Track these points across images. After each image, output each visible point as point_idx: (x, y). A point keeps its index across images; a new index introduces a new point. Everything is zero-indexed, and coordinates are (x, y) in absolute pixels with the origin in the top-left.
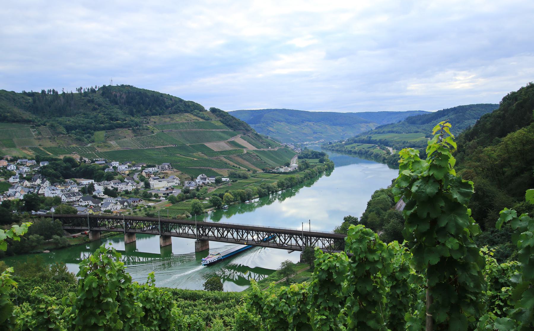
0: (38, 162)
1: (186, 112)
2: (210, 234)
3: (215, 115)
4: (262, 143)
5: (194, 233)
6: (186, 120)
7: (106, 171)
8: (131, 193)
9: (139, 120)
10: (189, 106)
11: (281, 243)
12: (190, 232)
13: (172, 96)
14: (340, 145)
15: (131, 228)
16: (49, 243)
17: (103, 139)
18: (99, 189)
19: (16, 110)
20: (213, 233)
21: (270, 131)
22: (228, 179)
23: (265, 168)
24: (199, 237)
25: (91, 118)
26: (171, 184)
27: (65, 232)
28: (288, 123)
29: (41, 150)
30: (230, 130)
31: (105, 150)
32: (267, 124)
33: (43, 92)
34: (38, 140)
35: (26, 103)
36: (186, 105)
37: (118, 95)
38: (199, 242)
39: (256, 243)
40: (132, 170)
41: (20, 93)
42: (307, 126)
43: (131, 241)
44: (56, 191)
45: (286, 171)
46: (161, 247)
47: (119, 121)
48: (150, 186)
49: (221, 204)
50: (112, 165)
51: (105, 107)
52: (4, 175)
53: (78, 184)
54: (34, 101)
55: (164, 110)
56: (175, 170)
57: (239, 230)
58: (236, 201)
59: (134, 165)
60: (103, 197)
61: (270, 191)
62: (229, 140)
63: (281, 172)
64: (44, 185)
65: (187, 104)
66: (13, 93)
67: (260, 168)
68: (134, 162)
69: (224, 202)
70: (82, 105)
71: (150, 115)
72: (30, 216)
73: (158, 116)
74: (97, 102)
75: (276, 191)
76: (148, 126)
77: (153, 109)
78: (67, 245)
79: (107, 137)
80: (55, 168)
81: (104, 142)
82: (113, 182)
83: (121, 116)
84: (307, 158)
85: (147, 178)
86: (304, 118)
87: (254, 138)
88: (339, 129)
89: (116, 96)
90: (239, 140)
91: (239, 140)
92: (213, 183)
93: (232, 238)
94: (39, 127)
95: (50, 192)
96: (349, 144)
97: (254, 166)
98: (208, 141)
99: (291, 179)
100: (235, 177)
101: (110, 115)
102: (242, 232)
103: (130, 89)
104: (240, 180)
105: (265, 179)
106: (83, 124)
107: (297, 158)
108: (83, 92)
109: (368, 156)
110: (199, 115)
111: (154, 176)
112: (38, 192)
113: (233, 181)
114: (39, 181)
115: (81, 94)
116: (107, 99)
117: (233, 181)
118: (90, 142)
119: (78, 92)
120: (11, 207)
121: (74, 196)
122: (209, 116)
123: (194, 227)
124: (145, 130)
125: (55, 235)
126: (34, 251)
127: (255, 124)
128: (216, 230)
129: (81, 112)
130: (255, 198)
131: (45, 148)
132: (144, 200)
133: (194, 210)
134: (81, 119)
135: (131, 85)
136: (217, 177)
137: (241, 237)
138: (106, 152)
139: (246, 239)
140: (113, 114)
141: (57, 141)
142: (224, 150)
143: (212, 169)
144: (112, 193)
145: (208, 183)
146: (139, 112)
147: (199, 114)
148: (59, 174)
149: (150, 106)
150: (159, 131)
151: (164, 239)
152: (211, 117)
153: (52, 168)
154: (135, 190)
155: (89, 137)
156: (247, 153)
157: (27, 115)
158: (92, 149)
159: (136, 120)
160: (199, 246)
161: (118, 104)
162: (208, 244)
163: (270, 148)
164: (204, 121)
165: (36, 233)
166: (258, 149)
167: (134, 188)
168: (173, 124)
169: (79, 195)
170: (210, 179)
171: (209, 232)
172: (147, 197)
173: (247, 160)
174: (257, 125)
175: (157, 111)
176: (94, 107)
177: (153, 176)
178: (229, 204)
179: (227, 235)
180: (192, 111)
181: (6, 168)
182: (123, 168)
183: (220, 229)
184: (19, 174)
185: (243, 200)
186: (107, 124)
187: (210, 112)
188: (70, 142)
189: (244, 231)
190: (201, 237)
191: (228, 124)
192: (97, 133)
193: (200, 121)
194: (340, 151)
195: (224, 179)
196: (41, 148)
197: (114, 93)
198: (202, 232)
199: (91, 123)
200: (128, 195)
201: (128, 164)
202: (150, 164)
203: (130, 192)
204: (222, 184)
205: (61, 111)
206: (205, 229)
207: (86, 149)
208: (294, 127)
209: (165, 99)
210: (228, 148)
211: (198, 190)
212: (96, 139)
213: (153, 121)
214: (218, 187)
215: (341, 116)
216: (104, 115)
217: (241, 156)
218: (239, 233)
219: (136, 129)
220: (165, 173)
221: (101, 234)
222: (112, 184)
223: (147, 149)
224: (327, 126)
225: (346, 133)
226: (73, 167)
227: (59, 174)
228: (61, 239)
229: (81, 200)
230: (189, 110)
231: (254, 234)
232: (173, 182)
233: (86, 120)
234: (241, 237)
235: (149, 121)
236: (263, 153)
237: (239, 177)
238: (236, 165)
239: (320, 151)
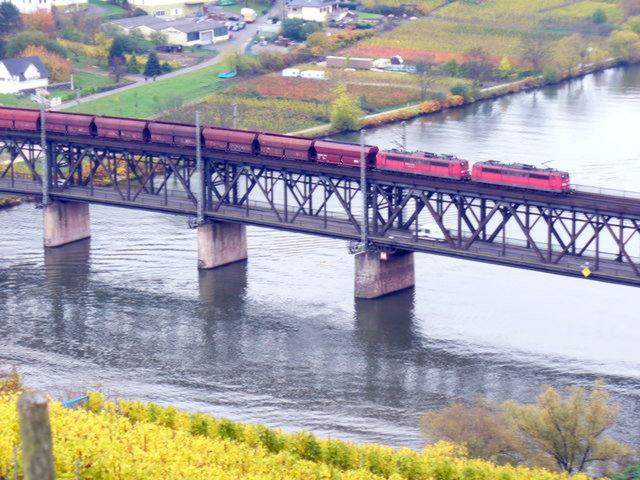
2: (257, 196)
11: (557, 248)
12: (335, 207)
15: (225, 200)
39: (280, 220)
57: (469, 200)
93: (347, 218)
102: (483, 207)
123: (272, 178)
137: (476, 226)
139: (321, 214)
162: (411, 268)
189: (490, 204)
198: (384, 213)
206: (401, 201)
218: (468, 213)
231: (533, 218)
234: (476, 226)
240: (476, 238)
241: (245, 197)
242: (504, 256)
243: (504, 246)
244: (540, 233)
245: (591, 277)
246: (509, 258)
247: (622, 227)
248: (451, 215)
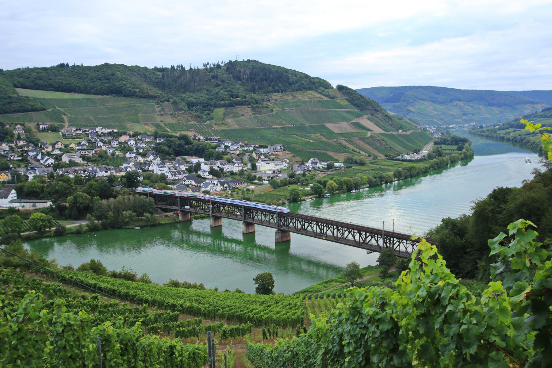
0: (156, 138)
1: (310, 89)
3: (341, 94)
4: (391, 125)
5: (333, 235)
6: (309, 98)
7: (216, 150)
8: (236, 174)
9: (260, 97)
10: (314, 83)
12: (374, 242)
13: (298, 72)
14: (492, 130)
16: (142, 220)
17: (222, 117)
18: (206, 167)
19: (145, 86)
20: (332, 232)
21: (411, 111)
22: (342, 165)
23: (388, 154)
24: (280, 227)
25: (213, 95)
26: (278, 167)
27: (159, 211)
28: (434, 102)
29: (162, 126)
30: (356, 110)
31: (222, 129)
32: (408, 103)
33: (173, 67)
34: (160, 116)
35: (156, 78)
36: (310, 82)
37: (242, 71)
38: (278, 233)
40: (243, 150)
41: (152, 69)
42: (456, 106)
43: (217, 225)
44: (164, 169)
45: (411, 159)
46: (244, 234)
47: (239, 99)
48: (256, 168)
49: (322, 192)
50: (224, 144)
51: (227, 83)
52: (123, 150)
53: (188, 162)
54: (163, 77)
55: (287, 87)
56: (287, 152)
58: (342, 189)
59: (246, 145)
60: (207, 177)
61: (383, 181)
62: (353, 121)
63: (406, 159)
64: (156, 162)
65: (312, 80)
66: (145, 69)
67: (383, 154)
68: (246, 142)
69: (327, 190)
70: (207, 81)
71: (272, 92)
72: (128, 193)
73: (280, 94)
74: (220, 78)
75: (391, 182)
76: (269, 104)
77: (276, 86)
78: (157, 223)
79: (225, 115)
80: (169, 145)
81: (223, 120)
82: (220, 162)
83: (241, 93)
84: (445, 144)
85: (256, 160)
86: (453, 97)
87: (383, 120)
88: (496, 110)
89: (240, 72)
90: (364, 121)
91: (364, 121)
92: (324, 168)
94: (163, 103)
95: (158, 169)
96: (504, 129)
97: (376, 151)
98: (330, 122)
99: (410, 169)
100: (351, 163)
101: (231, 91)
102: (366, 235)
103: (255, 64)
104: (355, 166)
105: (384, 167)
106: (204, 100)
107: (433, 143)
108: (208, 67)
109: (523, 144)
110: (323, 93)
111: (264, 157)
112: (148, 168)
113: (347, 167)
114: (151, 158)
115: (206, 69)
116: (231, 75)
117: (347, 167)
118: (208, 119)
119: (204, 68)
120: (115, 182)
121: (180, 174)
122: (334, 94)
124: (265, 109)
125: (146, 212)
126: (127, 227)
127: (394, 102)
128: (358, 234)
129: (204, 88)
130: (364, 188)
131: (166, 125)
132: (247, 182)
133: (292, 196)
134: (203, 95)
135: (257, 60)
136: (329, 162)
138: (222, 130)
140: (234, 90)
141: (178, 118)
142: (346, 132)
143: (328, 153)
144: (216, 173)
145: (319, 168)
146: (260, 88)
147: (324, 91)
148: (171, 150)
149: (273, 83)
150: (279, 109)
151: (246, 226)
152: (337, 96)
153: (167, 145)
154: (240, 172)
155: (209, 114)
156: (371, 136)
157: (154, 91)
158: (210, 126)
159: (256, 96)
160: (279, 236)
161: (241, 81)
162: (289, 235)
163: (400, 131)
164: (329, 99)
165: (130, 209)
166: (387, 131)
167: (240, 169)
168: (294, 102)
169: (184, 173)
170: (323, 163)
171: (327, 231)
172: (251, 179)
173: (369, 145)
174: (396, 104)
175: (279, 87)
176: (217, 83)
177: (263, 157)
178: (332, 193)
179: (348, 236)
180: (316, 88)
181: (127, 143)
182: (234, 148)
183: (362, 232)
184: (136, 149)
185: (349, 190)
186: (227, 101)
187: (337, 90)
188: (189, 118)
190: (282, 227)
191: (355, 103)
192: (216, 110)
193: (324, 99)
194: (490, 137)
195: (336, 164)
196: (162, 125)
197: (239, 68)
199: (212, 100)
200: (233, 176)
201: (241, 143)
202: (263, 144)
203: (236, 173)
204: (333, 169)
205: (185, 88)
207: (203, 127)
208: (440, 107)
209: (290, 75)
210: (351, 130)
211: (304, 175)
212: (215, 116)
213: (274, 99)
214: (328, 173)
215: (500, 95)
216: (226, 91)
217: (363, 139)
219: (255, 105)
220: (276, 155)
221: (191, 215)
222: (219, 164)
223: (263, 128)
224: (481, 107)
225: (504, 116)
226: (186, 144)
227: (171, 150)
228: (151, 217)
229: (185, 178)
230: (314, 88)
231: (379, 239)
232: (281, 165)
233: (208, 96)
235: (270, 99)
236: (392, 137)
237: (356, 163)
238: (355, 149)
239: (462, 136)
240: (364, 242)
241: (326, 232)
242: (327, 238)
243: (371, 245)
244: (263, 218)
245: (325, 239)
246: (349, 243)
247: (406, 243)
248: (357, 237)
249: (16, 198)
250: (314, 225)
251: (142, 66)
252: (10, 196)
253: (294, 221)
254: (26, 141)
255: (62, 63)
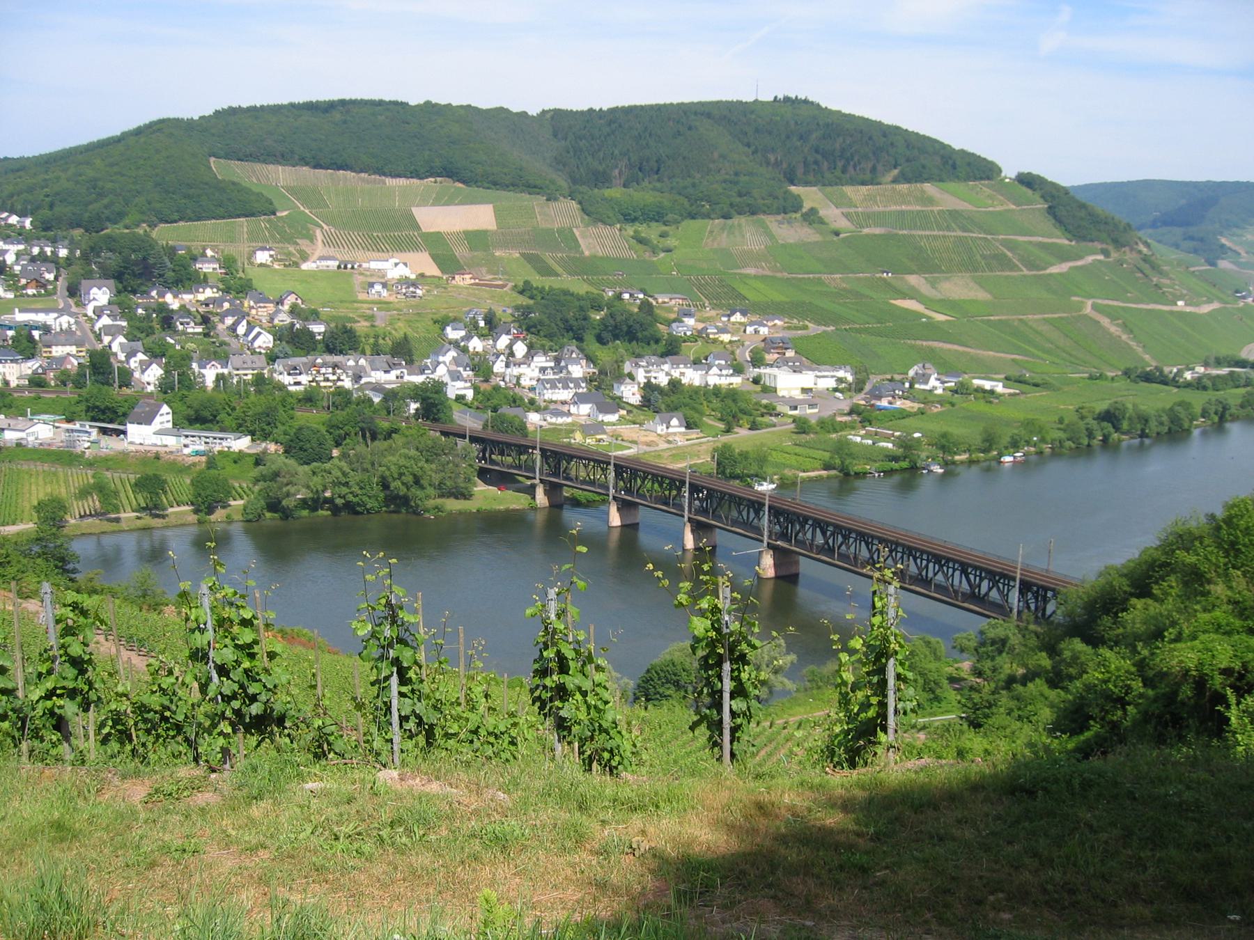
162: (797, 563)
249: (170, 425)
250: (954, 570)
251: (515, 109)
252: (158, 419)
253: (851, 540)
254: (219, 290)
255: (1000, 165)
